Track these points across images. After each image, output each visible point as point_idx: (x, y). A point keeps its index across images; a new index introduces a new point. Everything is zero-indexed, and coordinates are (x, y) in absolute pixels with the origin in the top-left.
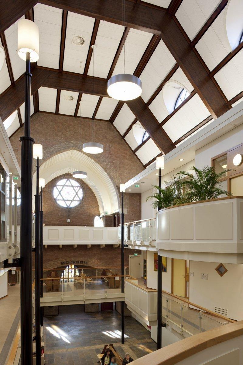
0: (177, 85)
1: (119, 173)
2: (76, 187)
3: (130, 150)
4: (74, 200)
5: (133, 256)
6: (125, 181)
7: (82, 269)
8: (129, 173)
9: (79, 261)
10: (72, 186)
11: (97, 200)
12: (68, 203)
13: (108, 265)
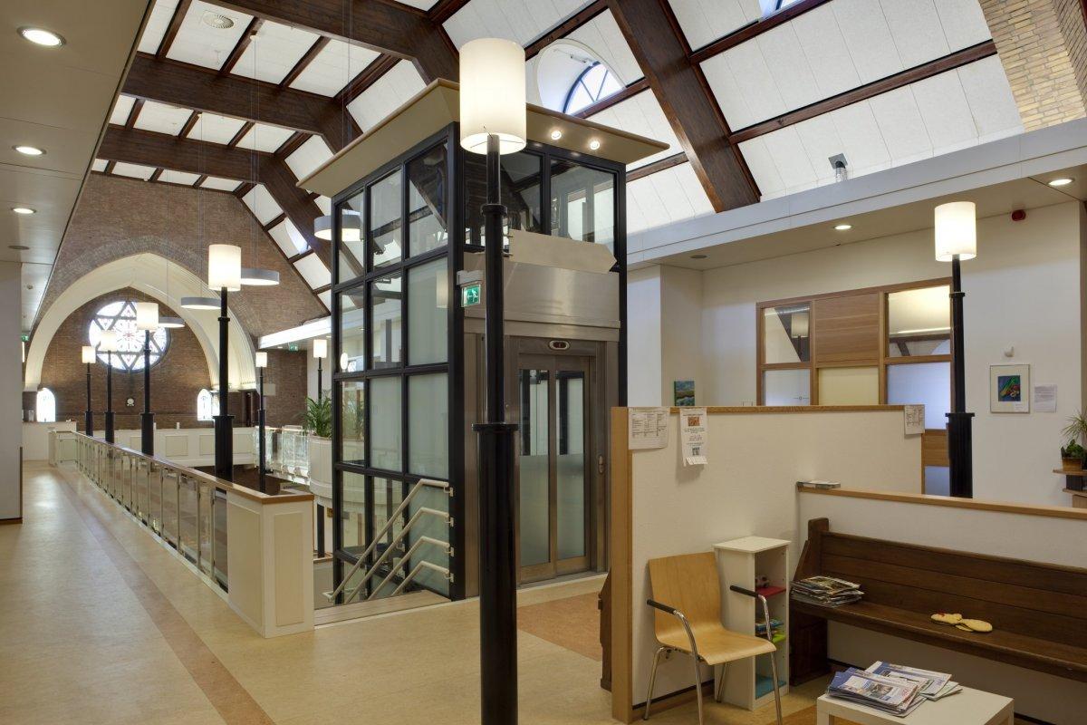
0: (583, 53)
3: (282, 256)
4: (135, 356)
11: (203, 353)
12: (128, 360)
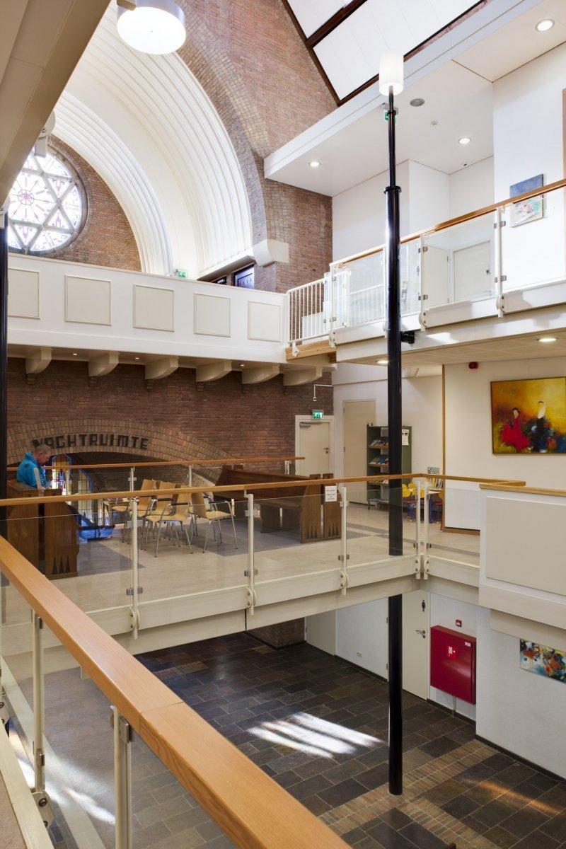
1: (262, 107)
2: (56, 178)
4: (50, 224)
5: (307, 418)
6: (281, 141)
7: (128, 469)
8: (295, 115)
9: (112, 436)
10: (42, 174)
13: (225, 455)
